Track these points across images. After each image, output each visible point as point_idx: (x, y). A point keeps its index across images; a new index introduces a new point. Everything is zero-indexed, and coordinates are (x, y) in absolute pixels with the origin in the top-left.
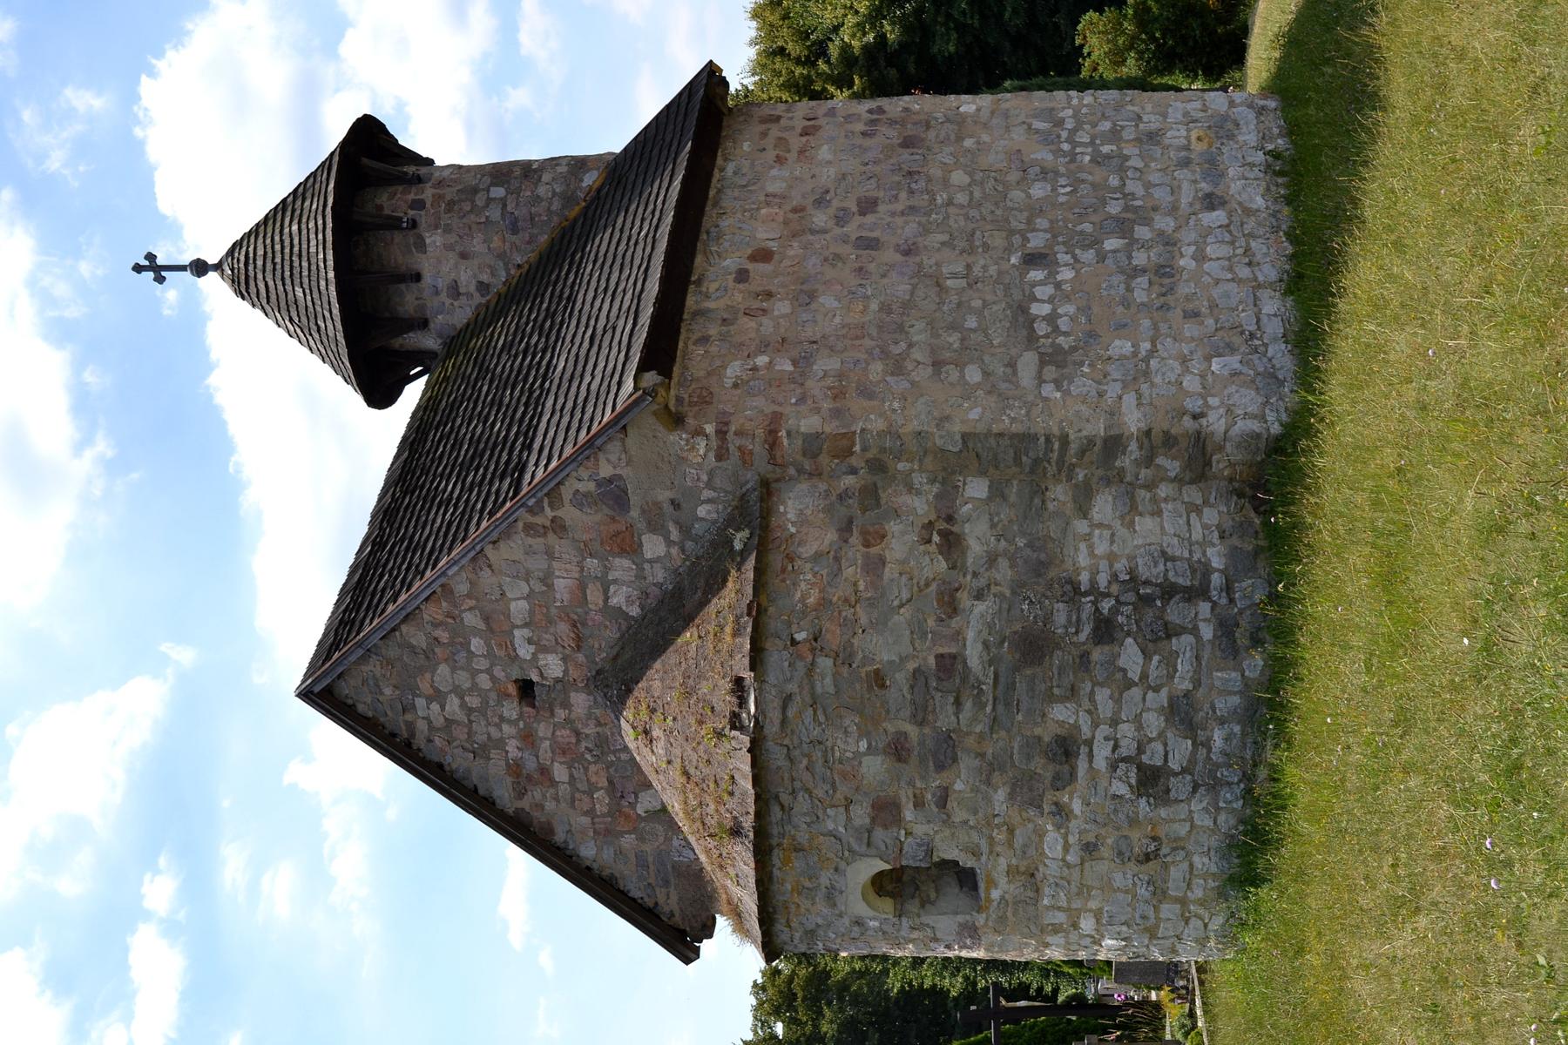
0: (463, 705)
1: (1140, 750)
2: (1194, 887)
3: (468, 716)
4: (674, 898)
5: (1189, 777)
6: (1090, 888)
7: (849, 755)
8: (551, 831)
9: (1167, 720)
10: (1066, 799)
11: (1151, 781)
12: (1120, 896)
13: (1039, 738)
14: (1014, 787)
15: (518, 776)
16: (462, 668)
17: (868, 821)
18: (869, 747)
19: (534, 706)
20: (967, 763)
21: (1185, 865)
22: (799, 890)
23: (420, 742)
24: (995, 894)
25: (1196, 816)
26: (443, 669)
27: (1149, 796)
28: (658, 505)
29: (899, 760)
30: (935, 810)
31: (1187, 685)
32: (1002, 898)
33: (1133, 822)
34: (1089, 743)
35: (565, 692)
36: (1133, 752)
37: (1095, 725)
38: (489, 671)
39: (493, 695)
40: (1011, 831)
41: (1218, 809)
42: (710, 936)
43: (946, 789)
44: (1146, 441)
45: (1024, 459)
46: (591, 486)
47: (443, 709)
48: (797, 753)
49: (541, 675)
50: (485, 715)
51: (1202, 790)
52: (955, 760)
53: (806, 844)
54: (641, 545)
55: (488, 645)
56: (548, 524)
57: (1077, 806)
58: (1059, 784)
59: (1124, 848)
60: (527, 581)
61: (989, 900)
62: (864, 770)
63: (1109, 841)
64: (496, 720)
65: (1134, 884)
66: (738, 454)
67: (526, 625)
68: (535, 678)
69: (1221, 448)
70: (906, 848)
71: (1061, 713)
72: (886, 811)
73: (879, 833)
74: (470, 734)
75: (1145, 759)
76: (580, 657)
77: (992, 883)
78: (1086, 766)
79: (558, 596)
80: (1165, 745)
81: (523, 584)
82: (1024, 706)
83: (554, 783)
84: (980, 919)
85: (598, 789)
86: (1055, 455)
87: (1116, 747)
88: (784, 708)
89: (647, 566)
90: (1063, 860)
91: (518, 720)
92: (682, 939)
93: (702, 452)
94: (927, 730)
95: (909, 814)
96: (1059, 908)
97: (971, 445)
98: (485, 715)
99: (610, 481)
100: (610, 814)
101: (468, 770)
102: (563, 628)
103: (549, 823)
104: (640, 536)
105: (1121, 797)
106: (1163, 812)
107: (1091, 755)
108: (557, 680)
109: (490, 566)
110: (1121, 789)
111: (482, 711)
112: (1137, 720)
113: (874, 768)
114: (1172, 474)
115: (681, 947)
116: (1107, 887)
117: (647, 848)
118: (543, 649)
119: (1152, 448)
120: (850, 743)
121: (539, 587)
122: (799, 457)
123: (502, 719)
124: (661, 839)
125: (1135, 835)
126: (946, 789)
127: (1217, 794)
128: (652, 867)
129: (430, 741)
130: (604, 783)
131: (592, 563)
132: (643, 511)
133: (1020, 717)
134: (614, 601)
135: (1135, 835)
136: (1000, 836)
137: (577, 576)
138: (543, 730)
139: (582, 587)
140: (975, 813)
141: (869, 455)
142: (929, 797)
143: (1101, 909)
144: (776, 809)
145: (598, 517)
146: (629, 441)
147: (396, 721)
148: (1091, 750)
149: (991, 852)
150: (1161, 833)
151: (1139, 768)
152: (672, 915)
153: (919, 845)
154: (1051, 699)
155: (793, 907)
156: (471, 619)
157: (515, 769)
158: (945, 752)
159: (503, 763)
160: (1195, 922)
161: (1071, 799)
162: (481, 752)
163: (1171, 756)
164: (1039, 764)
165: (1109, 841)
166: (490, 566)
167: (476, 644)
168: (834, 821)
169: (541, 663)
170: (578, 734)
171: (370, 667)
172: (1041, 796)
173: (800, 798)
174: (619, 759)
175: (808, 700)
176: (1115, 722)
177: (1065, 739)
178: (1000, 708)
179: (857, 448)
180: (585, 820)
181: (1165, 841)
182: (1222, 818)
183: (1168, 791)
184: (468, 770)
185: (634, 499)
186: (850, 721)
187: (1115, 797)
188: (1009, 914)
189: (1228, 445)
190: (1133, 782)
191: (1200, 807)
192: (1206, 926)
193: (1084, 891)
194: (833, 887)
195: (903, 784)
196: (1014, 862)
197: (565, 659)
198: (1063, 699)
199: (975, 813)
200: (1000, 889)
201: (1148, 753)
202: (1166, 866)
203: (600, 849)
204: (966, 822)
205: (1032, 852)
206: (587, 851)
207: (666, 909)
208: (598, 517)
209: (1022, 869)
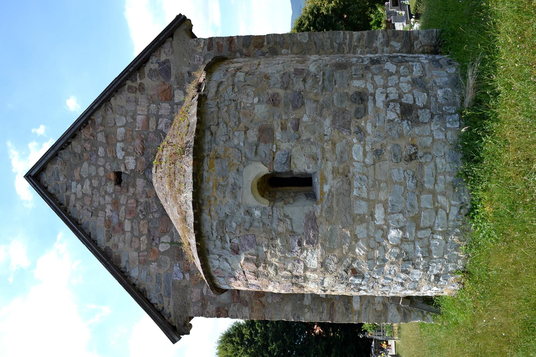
0: (91, 185)
1: (400, 96)
2: (439, 182)
3: (92, 191)
4: (172, 304)
5: (428, 111)
6: (380, 182)
7: (248, 105)
8: (120, 261)
9: (412, 86)
10: (363, 124)
11: (407, 111)
12: (397, 187)
13: (347, 93)
14: (335, 116)
15: (109, 227)
16: (93, 164)
17: (256, 139)
18: (259, 101)
19: (120, 186)
20: (309, 106)
21: (432, 165)
22: (217, 186)
23: (70, 208)
24: (326, 188)
25: (435, 133)
26: (85, 165)
27: (408, 120)
28: (182, 74)
29: (274, 105)
30: (292, 132)
31: (419, 74)
32: (330, 191)
33: (401, 135)
34: (373, 95)
35: (135, 178)
36: (396, 97)
37: (376, 88)
38: (104, 166)
39: (104, 179)
40: (334, 144)
41: (446, 128)
42: (188, 333)
43: (299, 120)
44: (385, 34)
45: (335, 44)
46: (157, 66)
47: (82, 188)
48: (222, 105)
49: (125, 168)
50: (99, 191)
51: (436, 117)
52: (303, 104)
53: (222, 153)
54: (174, 96)
55: (105, 151)
56: (137, 87)
57: (369, 128)
58: (359, 115)
59: (397, 151)
60: (126, 117)
61: (322, 193)
62: (255, 111)
63: (389, 148)
64: (103, 193)
65: (405, 178)
66: (216, 46)
67: (122, 141)
68: (122, 170)
69: (417, 38)
70: (276, 158)
71: (358, 84)
72: (266, 133)
73: (262, 148)
74: (92, 201)
75: (403, 100)
76: (143, 159)
77: (324, 180)
78: (373, 105)
79: (137, 125)
80: (413, 95)
81: (124, 118)
82: (338, 82)
83: (124, 232)
84: (318, 210)
85: (143, 235)
86: (347, 41)
87: (387, 97)
88: (218, 87)
89: (175, 106)
90: (364, 162)
91: (113, 193)
92: (175, 328)
93: (202, 46)
94: (289, 91)
95: (278, 135)
96: (363, 199)
97: (312, 38)
98: (99, 191)
99: (164, 63)
100: (146, 250)
101: (88, 223)
102: (138, 142)
103: (119, 256)
104: (174, 91)
105: (392, 121)
106: (417, 130)
107: (374, 100)
108: (132, 171)
109: (112, 108)
110: (392, 115)
111: (98, 189)
112: (397, 86)
113: (261, 110)
114: (398, 49)
115: (172, 333)
116: (390, 182)
117: (162, 272)
118: (128, 154)
119: (388, 37)
120: (249, 99)
121: (130, 120)
122: (241, 48)
123: (106, 192)
124: (169, 266)
125: (402, 143)
126: (299, 120)
127: (445, 119)
128: (163, 285)
129: (75, 206)
130: (145, 231)
131: (153, 106)
132: (176, 77)
133: (336, 86)
134: (160, 127)
135: (402, 143)
136: (328, 147)
137: (146, 113)
138: (123, 200)
139: (148, 120)
140: (314, 133)
141: (270, 45)
142: (289, 125)
143: (387, 200)
144: (208, 133)
145: (158, 83)
146: (174, 42)
147: (62, 196)
148: (374, 98)
149: (323, 158)
150: (417, 142)
151: (401, 104)
152: (170, 316)
153: (283, 155)
154: (351, 78)
155: (213, 199)
156: (101, 137)
157: (108, 222)
158: (298, 101)
159: (103, 219)
160: (442, 213)
161: (366, 123)
162: (94, 213)
163: (417, 99)
164: (347, 105)
165: (389, 148)
166: (112, 108)
167: (101, 151)
168: (238, 140)
169: (126, 161)
170: (137, 201)
171: (57, 166)
172: (350, 122)
173: (221, 126)
174: (154, 216)
175: (231, 83)
176: (385, 87)
177: (360, 93)
178: (326, 83)
179: (265, 44)
180: (135, 254)
181: (420, 147)
182: (449, 134)
183: (418, 117)
184: (88, 223)
185: (173, 71)
186: (250, 90)
187: (390, 121)
188: (334, 204)
189: (420, 36)
190: (399, 112)
191: (436, 127)
192: (448, 215)
193: (375, 186)
194: (235, 184)
195: (276, 118)
196: (336, 165)
197: (136, 160)
198: (358, 79)
199: (314, 133)
200: (326, 186)
201: (405, 98)
202: (421, 165)
203: (140, 272)
204: (309, 140)
205: (345, 156)
206: (134, 273)
207: (167, 311)
208: (158, 83)
209: (341, 171)
